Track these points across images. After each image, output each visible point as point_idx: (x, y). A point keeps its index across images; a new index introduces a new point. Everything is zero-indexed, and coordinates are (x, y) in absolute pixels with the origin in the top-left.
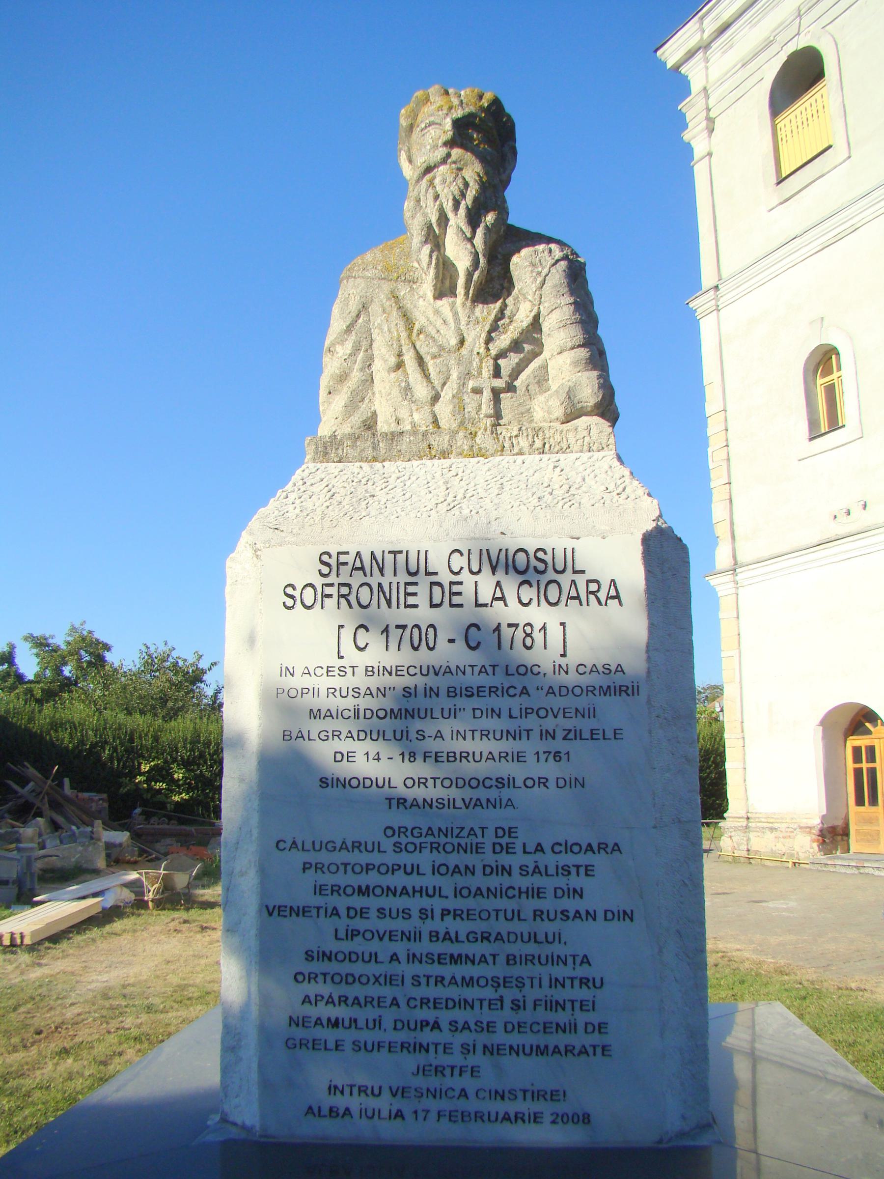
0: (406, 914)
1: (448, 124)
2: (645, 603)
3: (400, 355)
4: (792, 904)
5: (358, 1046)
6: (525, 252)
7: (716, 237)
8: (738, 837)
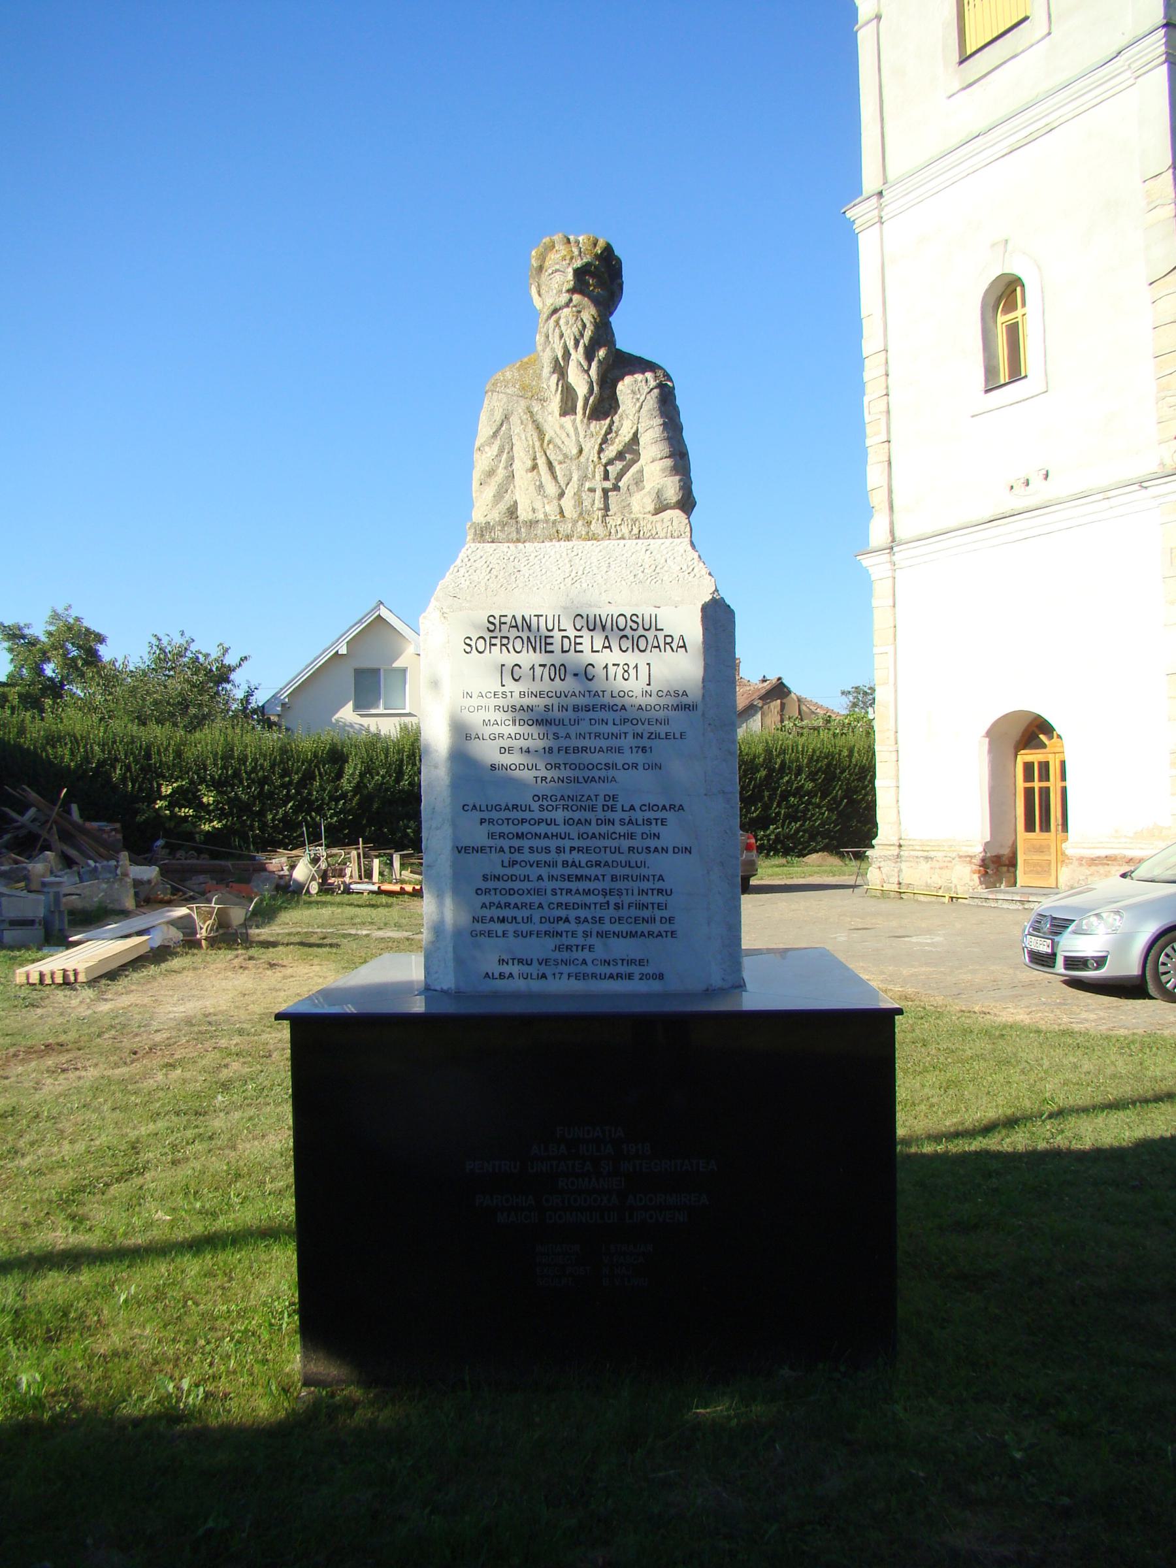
0: (547, 850)
1: (570, 275)
2: (702, 651)
3: (535, 459)
4: (937, 939)
5: (517, 934)
6: (628, 380)
7: (882, 128)
8: (888, 867)
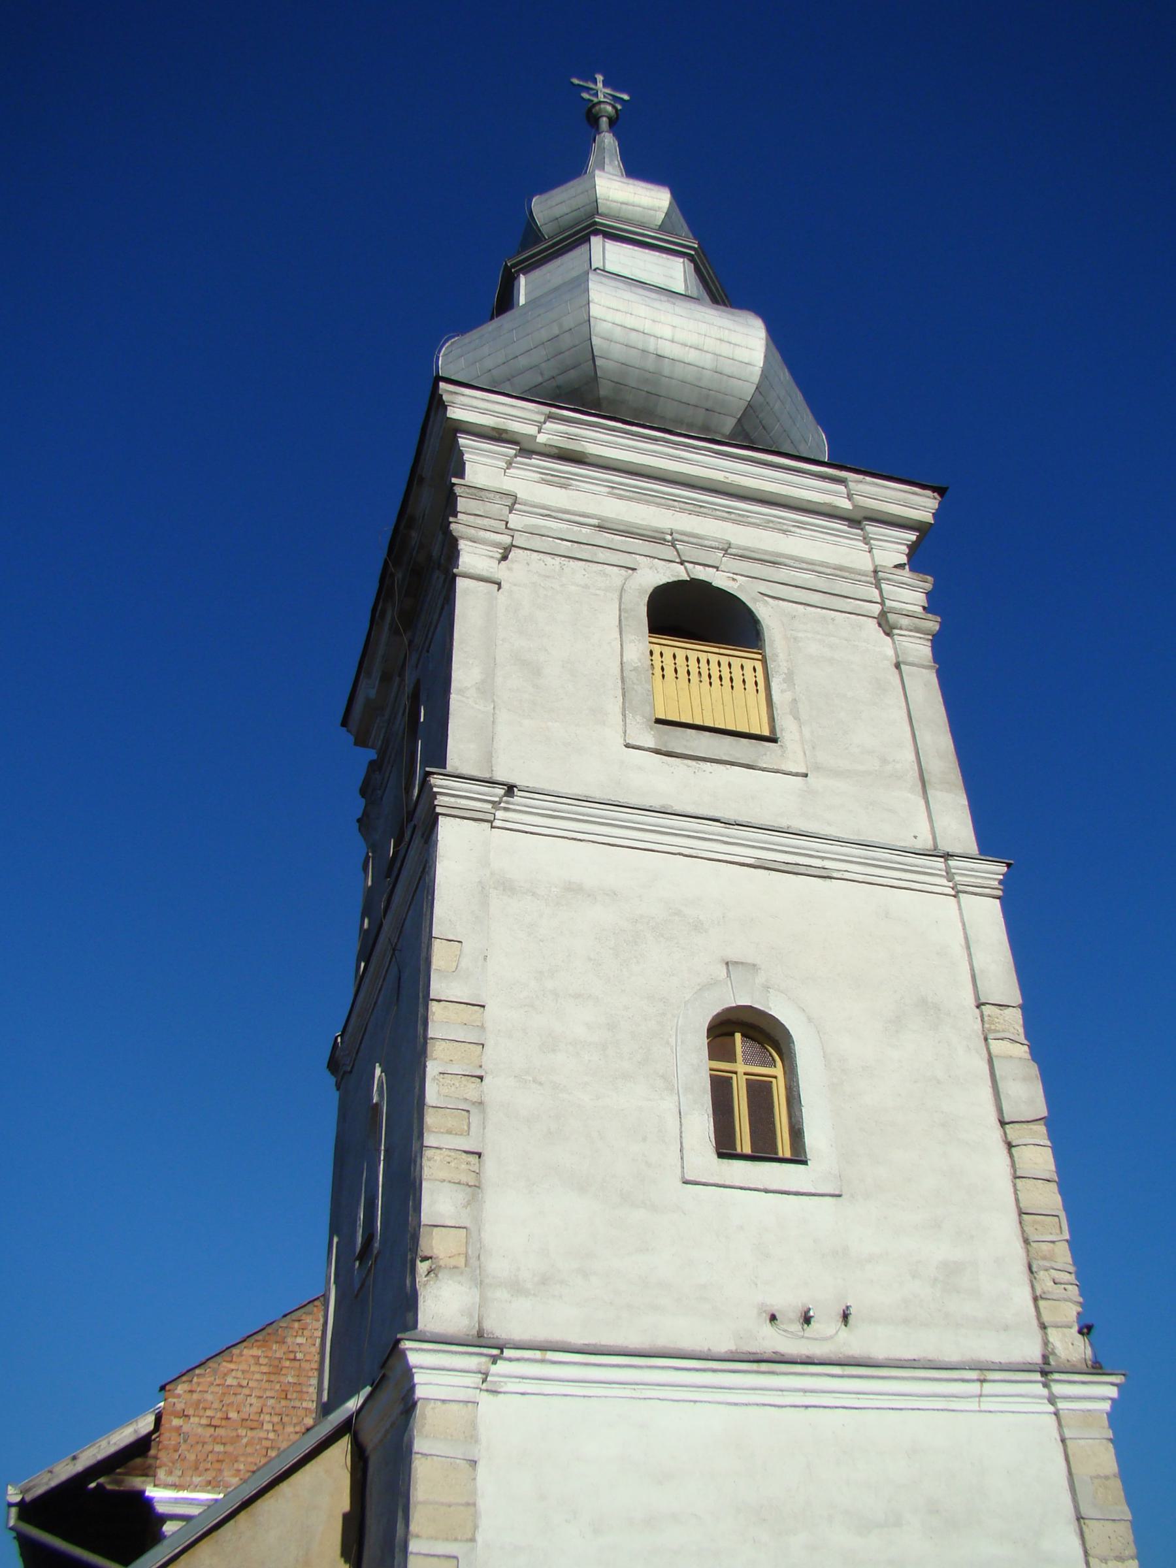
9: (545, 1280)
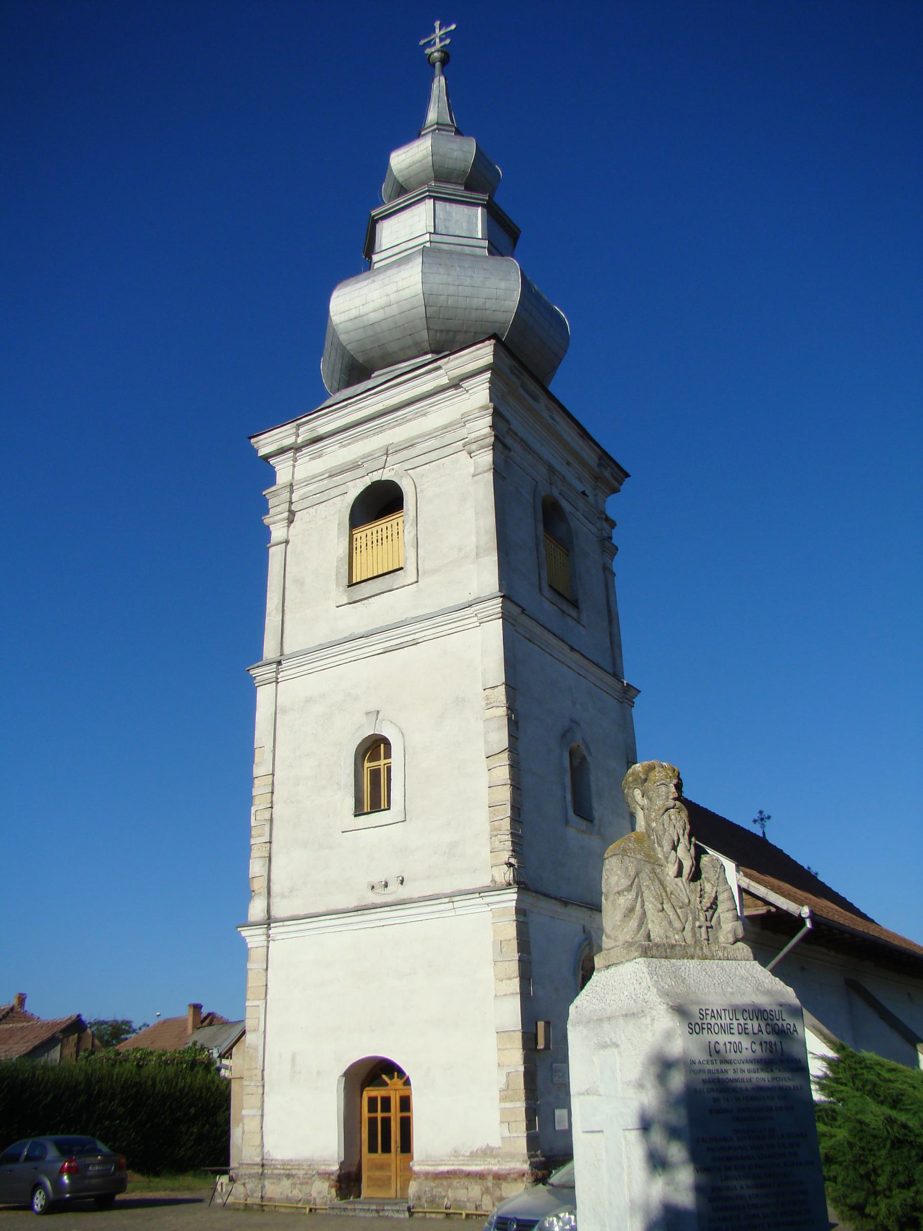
7: (283, 616)
9: (292, 890)
